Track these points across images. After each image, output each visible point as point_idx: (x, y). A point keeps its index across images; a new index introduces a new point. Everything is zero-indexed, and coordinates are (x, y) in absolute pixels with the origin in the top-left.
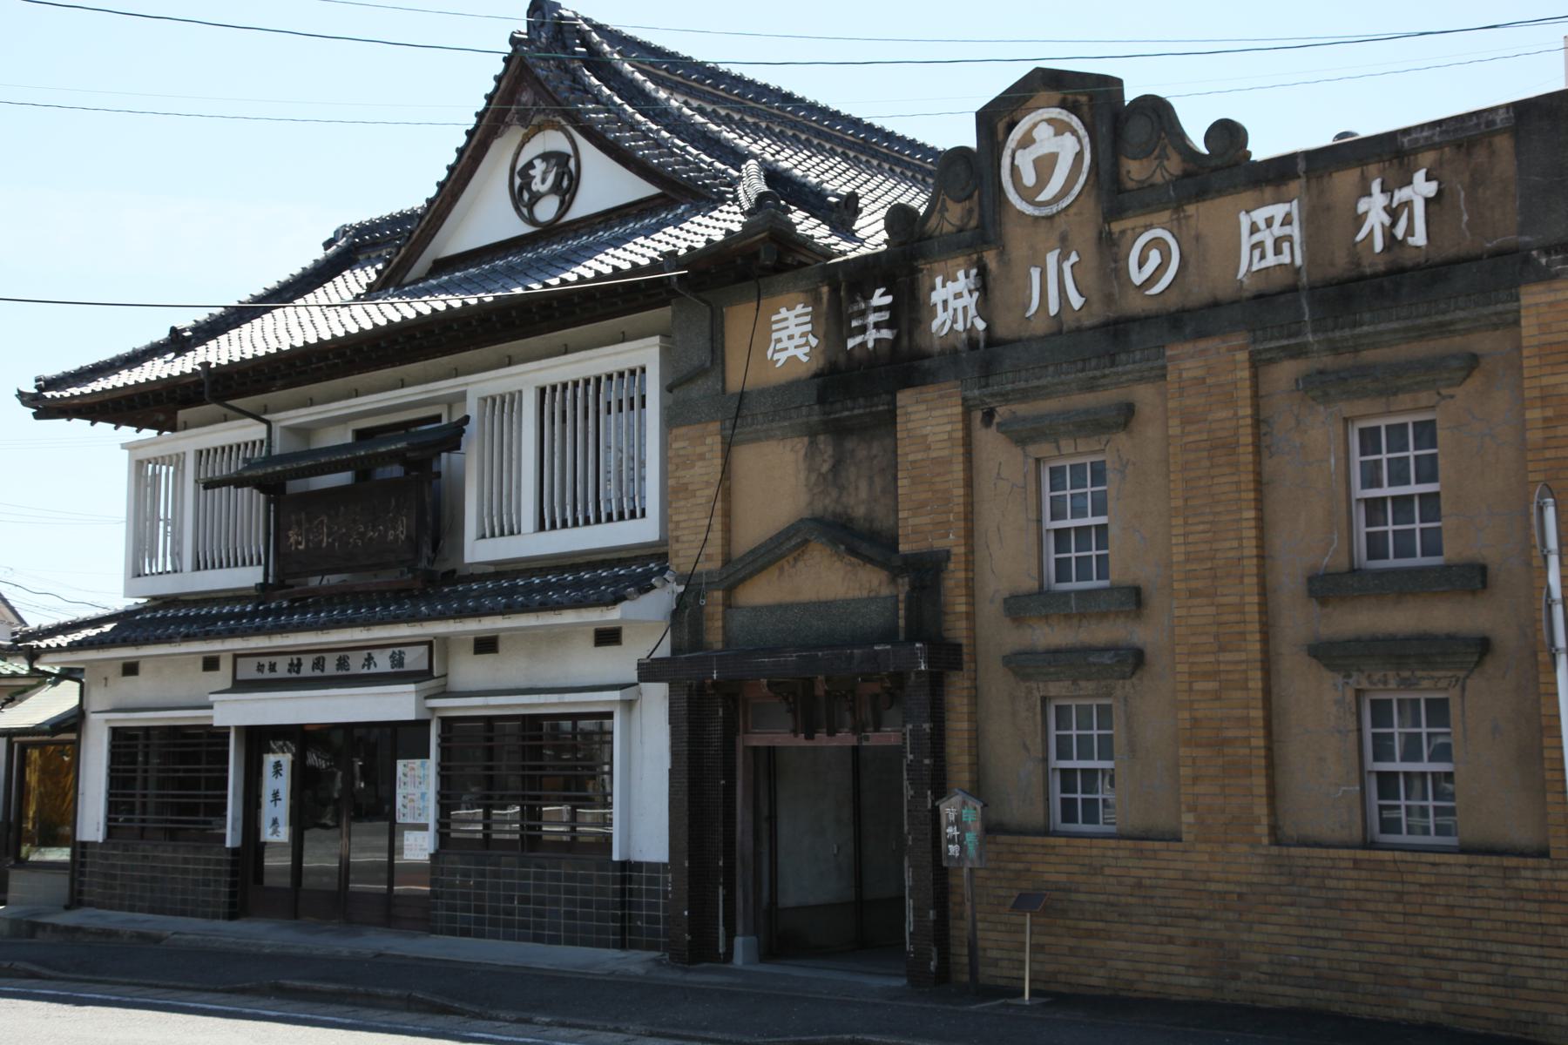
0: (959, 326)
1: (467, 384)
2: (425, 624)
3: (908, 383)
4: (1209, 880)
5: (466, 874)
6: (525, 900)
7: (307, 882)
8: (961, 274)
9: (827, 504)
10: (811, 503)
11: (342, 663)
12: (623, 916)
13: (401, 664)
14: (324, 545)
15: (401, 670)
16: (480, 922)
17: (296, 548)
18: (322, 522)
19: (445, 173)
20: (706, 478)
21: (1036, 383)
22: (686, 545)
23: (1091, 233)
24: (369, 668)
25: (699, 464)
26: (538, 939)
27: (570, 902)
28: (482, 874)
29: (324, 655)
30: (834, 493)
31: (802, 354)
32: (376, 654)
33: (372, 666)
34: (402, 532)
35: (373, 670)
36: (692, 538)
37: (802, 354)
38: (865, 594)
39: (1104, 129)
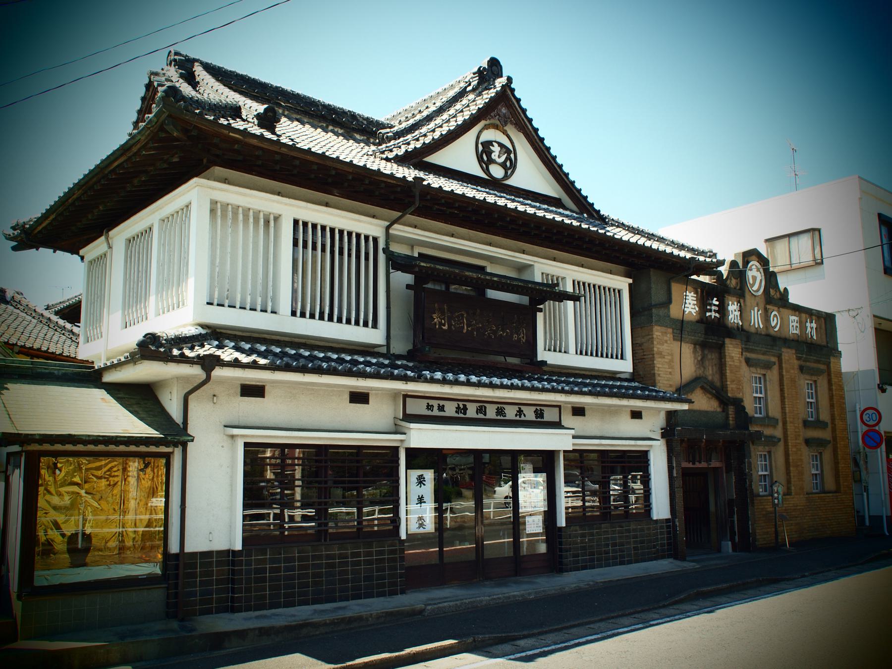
0: (736, 321)
1: (535, 262)
2: (599, 397)
3: (729, 337)
4: (797, 506)
5: (583, 536)
6: (614, 545)
7: (446, 560)
8: (736, 303)
9: (700, 372)
10: (695, 371)
11: (481, 410)
12: (233, 583)
13: (542, 416)
14: (465, 331)
15: (542, 420)
16: (592, 560)
17: (440, 328)
18: (462, 315)
19: (548, 145)
20: (668, 351)
21: (756, 348)
22: (662, 378)
23: (763, 306)
24: (520, 417)
25: (665, 344)
26: (622, 563)
27: (635, 542)
28: (592, 534)
29: (504, 406)
30: (702, 369)
31: (693, 311)
32: (468, 405)
33: (522, 416)
34: (523, 337)
35: (523, 418)
36: (664, 376)
37: (693, 311)
38: (712, 410)
39: (768, 276)
